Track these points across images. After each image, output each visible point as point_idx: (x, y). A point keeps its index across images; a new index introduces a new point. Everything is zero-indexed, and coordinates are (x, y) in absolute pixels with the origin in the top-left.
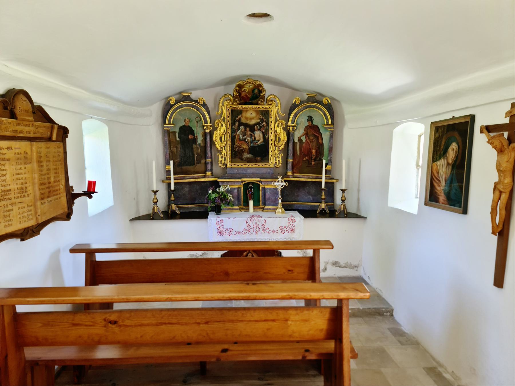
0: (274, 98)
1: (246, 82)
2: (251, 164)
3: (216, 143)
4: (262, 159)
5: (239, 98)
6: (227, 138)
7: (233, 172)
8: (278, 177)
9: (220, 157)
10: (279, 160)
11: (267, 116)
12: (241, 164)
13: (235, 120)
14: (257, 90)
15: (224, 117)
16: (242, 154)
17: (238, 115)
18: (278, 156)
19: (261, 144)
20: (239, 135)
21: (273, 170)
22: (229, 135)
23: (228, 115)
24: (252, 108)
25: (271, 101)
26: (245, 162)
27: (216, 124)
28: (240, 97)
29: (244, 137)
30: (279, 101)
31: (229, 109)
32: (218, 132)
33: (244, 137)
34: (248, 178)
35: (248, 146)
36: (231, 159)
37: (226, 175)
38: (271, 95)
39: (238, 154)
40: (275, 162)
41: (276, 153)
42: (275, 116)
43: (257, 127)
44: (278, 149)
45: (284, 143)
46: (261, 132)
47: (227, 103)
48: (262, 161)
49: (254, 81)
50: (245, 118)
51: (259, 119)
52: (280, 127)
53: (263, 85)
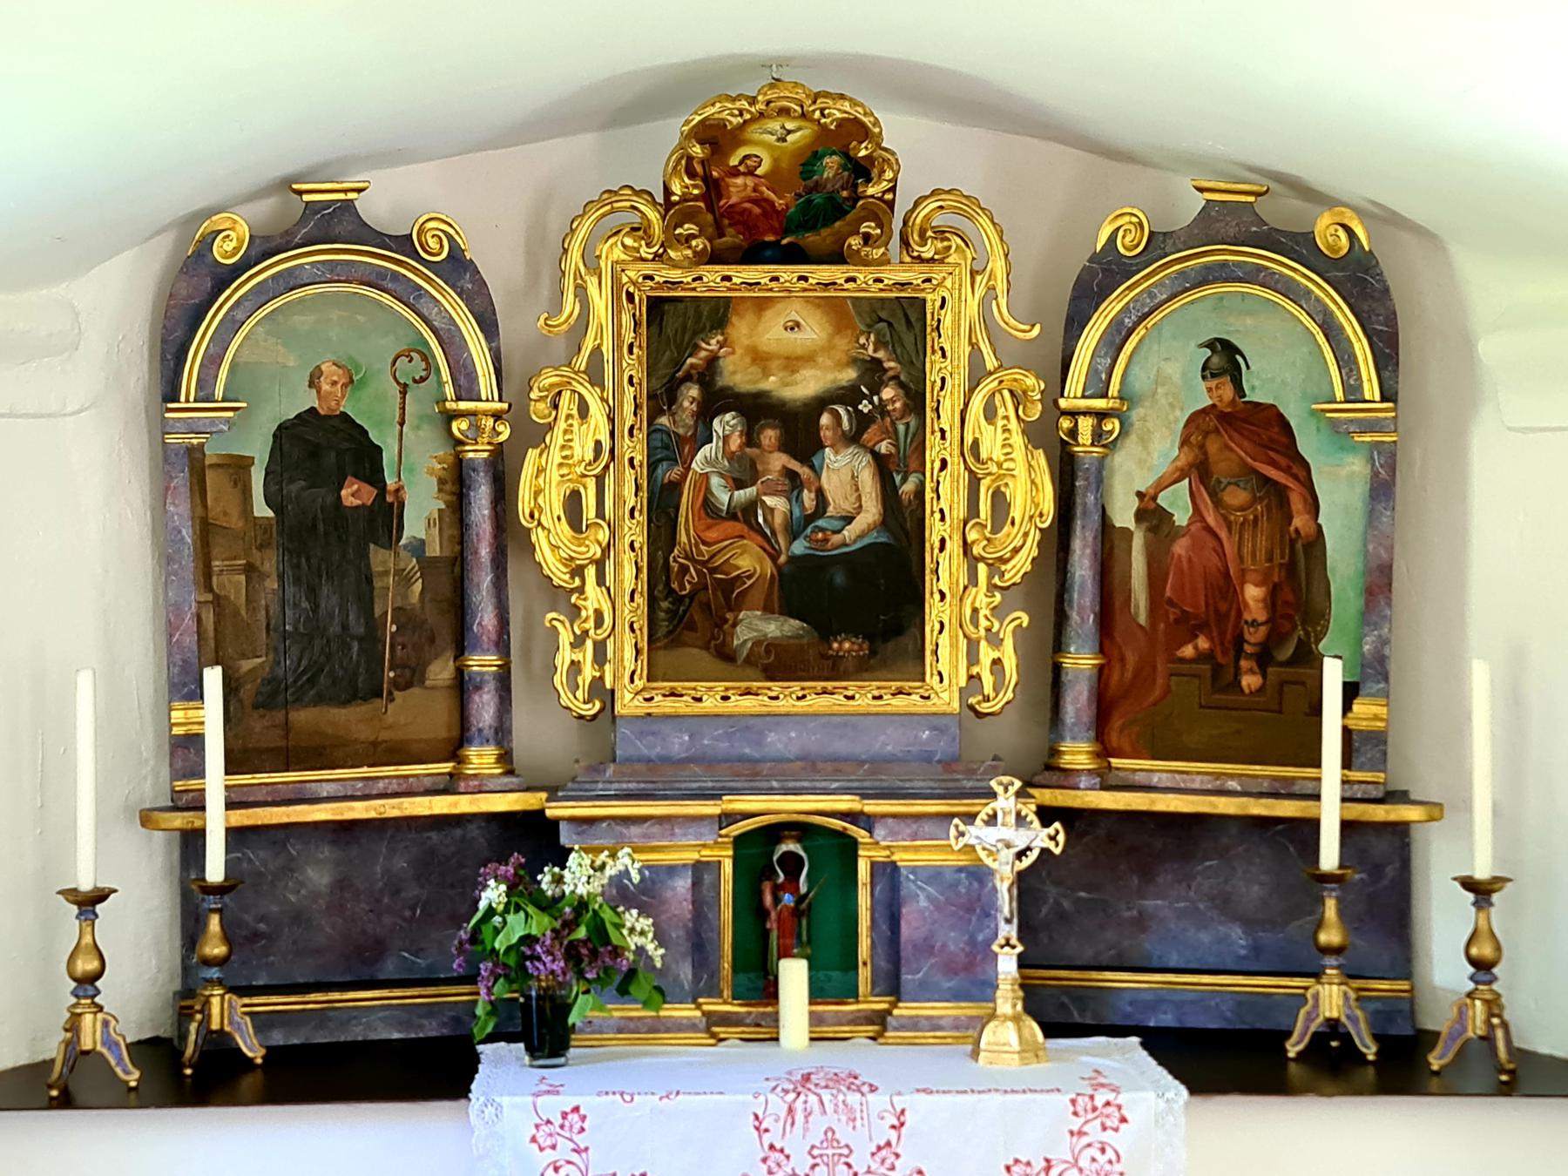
0: (959, 212)
1: (760, 106)
2: (796, 686)
3: (539, 537)
4: (873, 653)
5: (710, 217)
6: (619, 499)
7: (659, 749)
8: (993, 783)
9: (565, 637)
11: (908, 339)
15: (597, 351)
16: (729, 616)
17: (695, 334)
18: (988, 630)
19: (866, 541)
20: (706, 476)
21: (955, 730)
22: (629, 475)
23: (629, 337)
24: (803, 284)
25: (941, 234)
26: (749, 671)
27: (541, 399)
29: (742, 495)
30: (995, 239)
31: (630, 297)
32: (556, 456)
33: (742, 495)
34: (770, 791)
35: (774, 559)
37: (610, 770)
38: (934, 193)
40: (971, 677)
41: (975, 611)
44: (990, 577)
45: (1034, 536)
46: (869, 457)
47: (618, 254)
48: (884, 665)
49: (816, 97)
50: (748, 360)
51: (854, 361)
53: (876, 123)
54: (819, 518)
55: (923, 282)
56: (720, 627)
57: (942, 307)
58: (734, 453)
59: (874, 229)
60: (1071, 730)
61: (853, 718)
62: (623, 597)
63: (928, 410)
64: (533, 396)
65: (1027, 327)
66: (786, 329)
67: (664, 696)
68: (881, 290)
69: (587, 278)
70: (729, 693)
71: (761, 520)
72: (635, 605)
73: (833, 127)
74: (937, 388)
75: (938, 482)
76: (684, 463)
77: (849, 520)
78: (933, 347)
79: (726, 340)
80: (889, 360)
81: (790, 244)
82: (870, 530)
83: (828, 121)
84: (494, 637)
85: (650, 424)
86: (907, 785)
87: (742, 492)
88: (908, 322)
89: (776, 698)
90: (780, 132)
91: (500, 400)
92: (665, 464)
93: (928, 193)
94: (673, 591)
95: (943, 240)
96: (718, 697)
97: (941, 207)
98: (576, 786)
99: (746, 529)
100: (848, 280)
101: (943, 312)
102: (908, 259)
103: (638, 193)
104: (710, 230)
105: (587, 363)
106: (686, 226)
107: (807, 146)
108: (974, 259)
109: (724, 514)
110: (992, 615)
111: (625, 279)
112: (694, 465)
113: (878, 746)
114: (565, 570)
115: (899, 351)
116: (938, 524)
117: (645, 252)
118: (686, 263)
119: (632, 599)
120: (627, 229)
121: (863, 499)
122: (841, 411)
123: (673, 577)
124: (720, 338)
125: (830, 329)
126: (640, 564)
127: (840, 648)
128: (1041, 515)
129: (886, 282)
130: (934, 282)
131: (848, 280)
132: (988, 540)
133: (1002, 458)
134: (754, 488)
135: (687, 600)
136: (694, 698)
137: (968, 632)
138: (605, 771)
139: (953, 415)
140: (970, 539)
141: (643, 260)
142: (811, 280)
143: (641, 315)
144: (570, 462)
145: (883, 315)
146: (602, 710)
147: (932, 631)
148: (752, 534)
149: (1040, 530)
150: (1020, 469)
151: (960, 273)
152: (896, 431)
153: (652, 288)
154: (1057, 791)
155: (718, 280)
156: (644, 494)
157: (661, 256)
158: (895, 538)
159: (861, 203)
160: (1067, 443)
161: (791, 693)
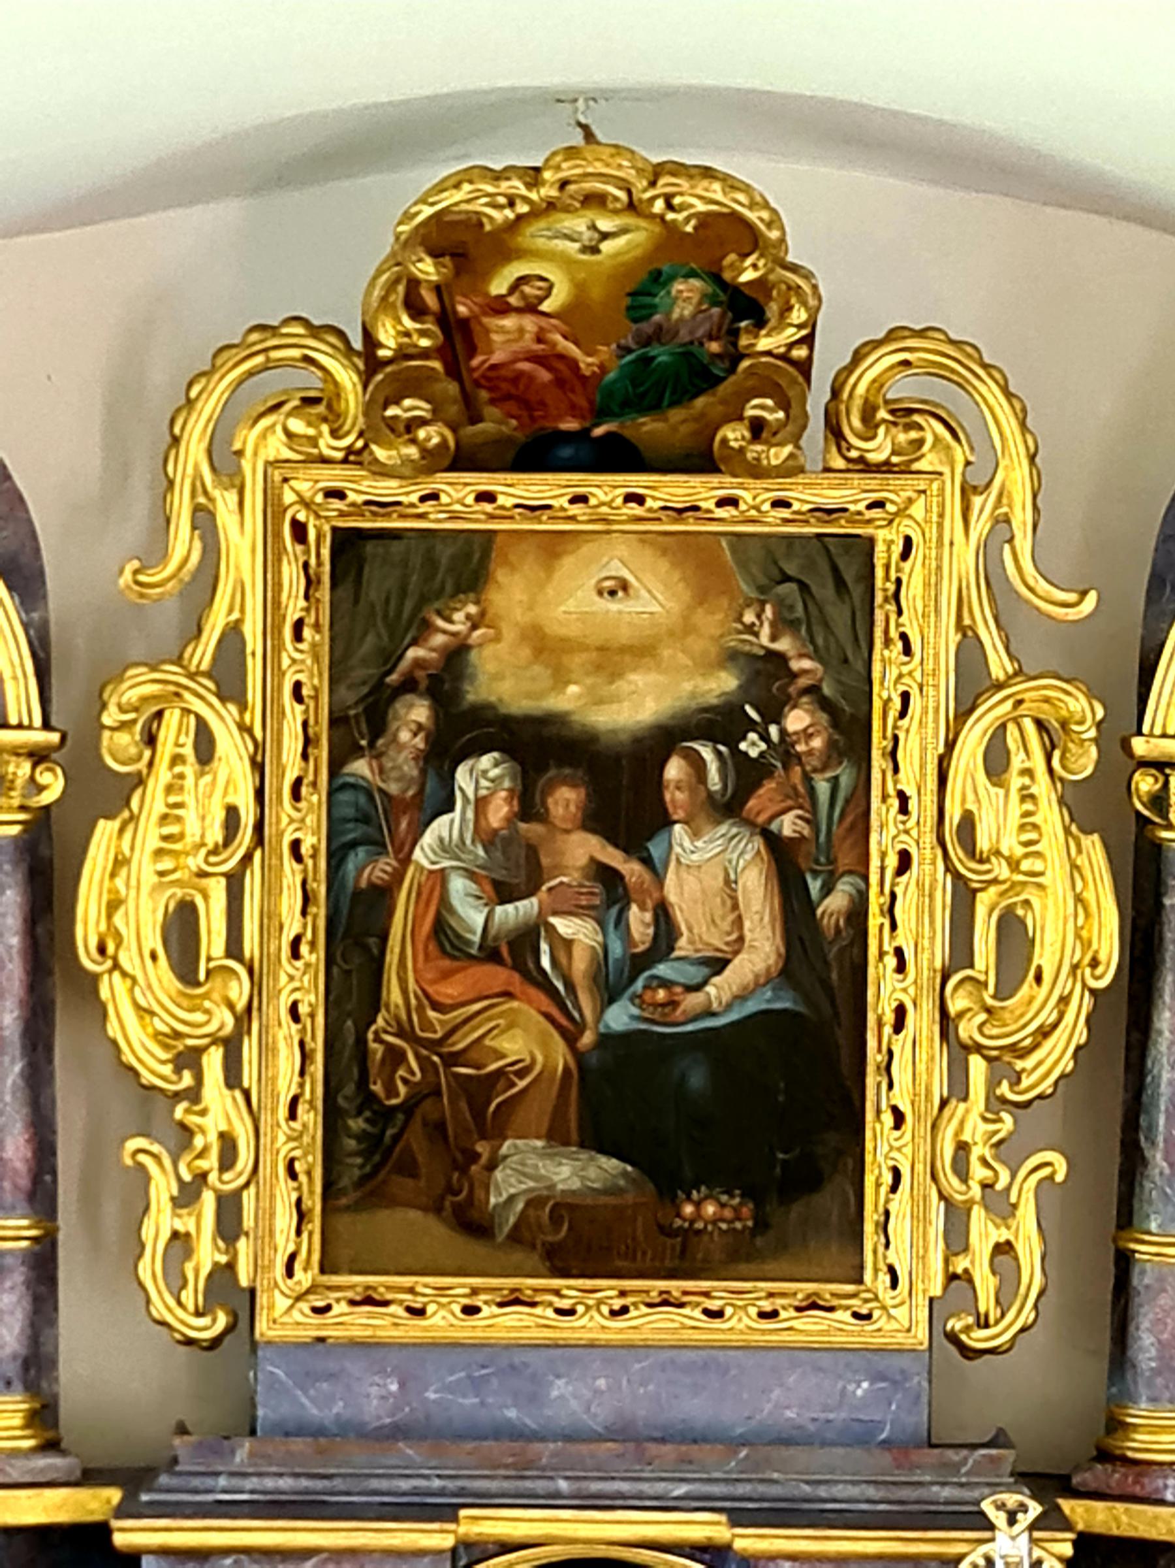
0: (938, 372)
1: (549, 191)
2: (608, 1287)
3: (112, 990)
4: (761, 1225)
5: (453, 388)
6: (270, 920)
7: (338, 1407)
8: (987, 1506)
9: (162, 1188)
10: (1004, 1249)
11: (839, 615)
12: (461, 1285)
13: (393, 678)
14: (695, 283)
15: (233, 634)
16: (482, 1148)
17: (424, 600)
18: (986, 1186)
19: (751, 1007)
20: (441, 877)
21: (919, 1381)
22: (291, 876)
23: (294, 608)
24: (634, 509)
25: (903, 414)
26: (518, 1256)
27: (123, 726)
28: (453, 371)
29: (511, 913)
30: (1010, 425)
31: (299, 532)
32: (150, 834)
33: (511, 913)
34: (551, 1501)
35: (570, 1039)
36: (316, 1225)
37: (243, 1451)
38: (893, 335)
39: (416, 1140)
40: (952, 1277)
41: (962, 1148)
42: (948, 619)
43: (698, 765)
44: (992, 1083)
45: (1080, 1007)
46: (758, 843)
47: (276, 447)
48: (781, 1248)
49: (656, 173)
50: (526, 652)
51: (732, 657)
52: (1028, 772)
53: (775, 221)
54: (660, 961)
55: (869, 507)
56: (464, 1170)
57: (905, 555)
58: (495, 832)
59: (771, 410)
60: (1150, 1384)
61: (720, 1354)
62: (274, 1111)
63: (876, 754)
64: (107, 719)
65: (1072, 597)
66: (600, 593)
67: (353, 1303)
68: (786, 521)
69: (216, 493)
70: (478, 1301)
71: (546, 962)
72: (296, 1125)
73: (689, 229)
74: (893, 714)
75: (893, 896)
76: (397, 852)
77: (718, 965)
78: (886, 631)
79: (483, 614)
80: (801, 656)
81: (609, 435)
82: (758, 985)
83: (680, 217)
84: (25, 1182)
85: (333, 772)
86: (822, 1492)
87: (510, 907)
88: (840, 584)
89: (571, 1312)
90: (587, 236)
91: (47, 726)
92: (361, 852)
93: (881, 335)
94: (372, 1097)
95: (908, 427)
96: (457, 1309)
97: (906, 363)
98: (174, 1482)
99: (516, 977)
100: (722, 503)
101: (907, 566)
102: (839, 463)
103: (316, 331)
104: (453, 410)
105: (215, 659)
106: (407, 402)
107: (649, 257)
108: (968, 463)
109: (474, 951)
110: (997, 1158)
111: (289, 497)
112: (417, 854)
113: (768, 1407)
114: (164, 1056)
115: (820, 641)
116: (891, 976)
117: (327, 445)
118: (407, 471)
119: (292, 1115)
120: (296, 403)
121: (747, 924)
122: (707, 753)
123: (373, 1070)
124: (472, 609)
125: (686, 596)
126: (309, 1045)
127: (698, 1215)
128: (1094, 963)
129: (796, 506)
130: (890, 508)
131: (722, 503)
132: (989, 1010)
133: (1019, 851)
134: (534, 900)
135: (400, 1117)
136: (410, 1310)
137: (947, 1190)
138: (233, 1452)
139: (923, 766)
140: (953, 1008)
141: (325, 460)
142: (649, 503)
143: (319, 564)
144: (177, 847)
145: (791, 569)
146: (229, 1330)
147: (878, 1185)
148: (533, 992)
149: (1093, 992)
150: (1056, 875)
151: (942, 490)
152: (812, 791)
153: (342, 514)
154: (1120, 1507)
155: (470, 500)
156: (320, 910)
157: (359, 452)
158: (807, 999)
159: (745, 364)
160: (1148, 821)
161: (600, 1302)
